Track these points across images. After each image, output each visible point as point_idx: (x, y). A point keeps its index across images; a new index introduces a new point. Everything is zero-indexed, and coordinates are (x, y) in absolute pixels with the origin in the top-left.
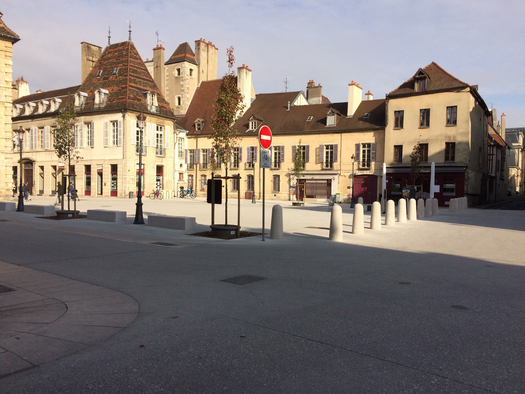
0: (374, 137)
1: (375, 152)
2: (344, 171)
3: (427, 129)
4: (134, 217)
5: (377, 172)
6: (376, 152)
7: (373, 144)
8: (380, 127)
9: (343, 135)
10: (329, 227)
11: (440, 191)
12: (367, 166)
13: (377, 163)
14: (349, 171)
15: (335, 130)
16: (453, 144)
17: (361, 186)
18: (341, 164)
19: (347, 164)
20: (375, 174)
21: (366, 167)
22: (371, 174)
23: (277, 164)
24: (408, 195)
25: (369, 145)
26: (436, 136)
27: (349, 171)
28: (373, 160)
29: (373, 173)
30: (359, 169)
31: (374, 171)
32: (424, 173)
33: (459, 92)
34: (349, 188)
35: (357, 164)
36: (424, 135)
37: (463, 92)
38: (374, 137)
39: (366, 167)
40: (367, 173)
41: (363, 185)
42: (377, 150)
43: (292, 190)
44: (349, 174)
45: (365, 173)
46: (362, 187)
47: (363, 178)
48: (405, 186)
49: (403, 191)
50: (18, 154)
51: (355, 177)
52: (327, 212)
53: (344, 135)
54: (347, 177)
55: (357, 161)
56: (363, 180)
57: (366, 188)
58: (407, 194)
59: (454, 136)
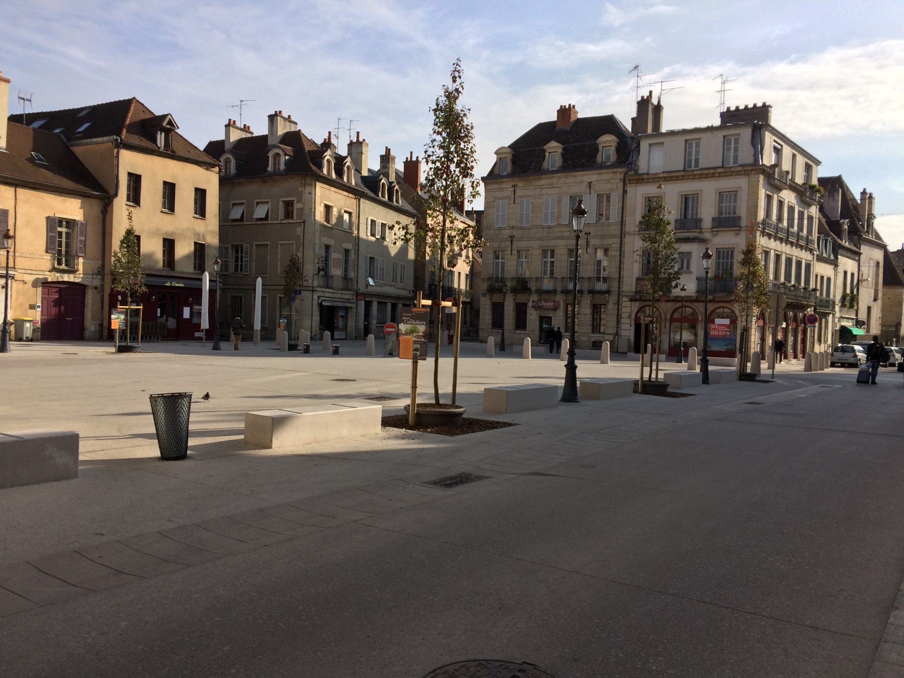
0: (82, 210)
1: (84, 238)
2: (23, 271)
3: (170, 215)
4: (562, 386)
5: (87, 279)
6: (85, 239)
7: (82, 224)
8: (100, 195)
9: (20, 191)
10: (659, 371)
11: (185, 319)
12: (65, 266)
13: (87, 261)
14: (32, 272)
15: (7, 178)
16: (202, 246)
17: (53, 304)
18: (16, 254)
19: (28, 255)
20: (85, 283)
21: (63, 267)
22: (77, 280)
23: (64, 259)
24: (120, 325)
25: (70, 223)
26: (183, 230)
27: (32, 272)
28: (82, 255)
29: (80, 280)
30: (54, 269)
31: (82, 276)
32: (175, 287)
33: (207, 169)
34: (32, 307)
35: (49, 258)
36: (168, 224)
37: (212, 171)
38: (82, 210)
39: (63, 267)
40: (70, 278)
41: (58, 303)
42: (88, 236)
43: (412, 332)
44: (33, 279)
45: (66, 278)
46: (55, 306)
47: (58, 287)
48: (116, 307)
49: (403, 327)
50: (618, 273)
51: (45, 284)
52: (383, 357)
53: (23, 193)
54: (29, 285)
55: (50, 251)
56: (55, 292)
57: (62, 308)
58: (119, 322)
59: (203, 235)
